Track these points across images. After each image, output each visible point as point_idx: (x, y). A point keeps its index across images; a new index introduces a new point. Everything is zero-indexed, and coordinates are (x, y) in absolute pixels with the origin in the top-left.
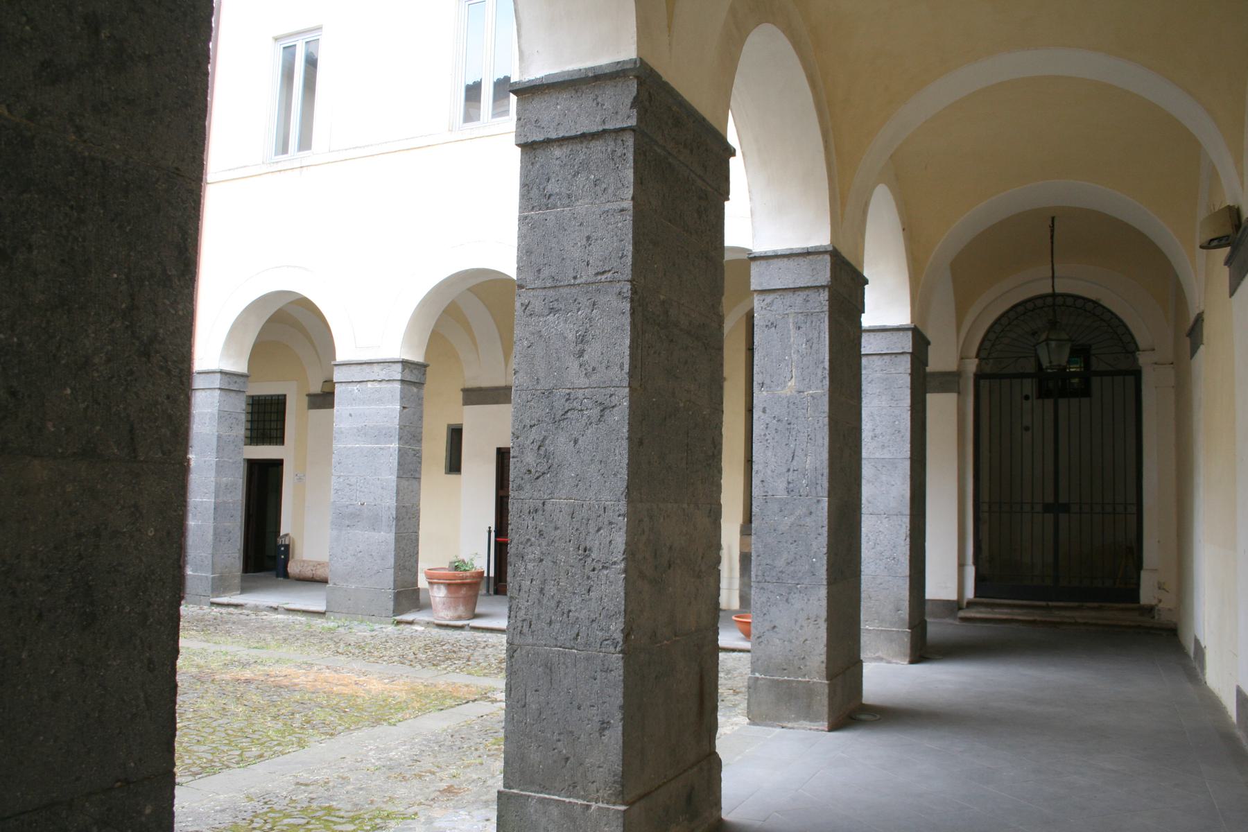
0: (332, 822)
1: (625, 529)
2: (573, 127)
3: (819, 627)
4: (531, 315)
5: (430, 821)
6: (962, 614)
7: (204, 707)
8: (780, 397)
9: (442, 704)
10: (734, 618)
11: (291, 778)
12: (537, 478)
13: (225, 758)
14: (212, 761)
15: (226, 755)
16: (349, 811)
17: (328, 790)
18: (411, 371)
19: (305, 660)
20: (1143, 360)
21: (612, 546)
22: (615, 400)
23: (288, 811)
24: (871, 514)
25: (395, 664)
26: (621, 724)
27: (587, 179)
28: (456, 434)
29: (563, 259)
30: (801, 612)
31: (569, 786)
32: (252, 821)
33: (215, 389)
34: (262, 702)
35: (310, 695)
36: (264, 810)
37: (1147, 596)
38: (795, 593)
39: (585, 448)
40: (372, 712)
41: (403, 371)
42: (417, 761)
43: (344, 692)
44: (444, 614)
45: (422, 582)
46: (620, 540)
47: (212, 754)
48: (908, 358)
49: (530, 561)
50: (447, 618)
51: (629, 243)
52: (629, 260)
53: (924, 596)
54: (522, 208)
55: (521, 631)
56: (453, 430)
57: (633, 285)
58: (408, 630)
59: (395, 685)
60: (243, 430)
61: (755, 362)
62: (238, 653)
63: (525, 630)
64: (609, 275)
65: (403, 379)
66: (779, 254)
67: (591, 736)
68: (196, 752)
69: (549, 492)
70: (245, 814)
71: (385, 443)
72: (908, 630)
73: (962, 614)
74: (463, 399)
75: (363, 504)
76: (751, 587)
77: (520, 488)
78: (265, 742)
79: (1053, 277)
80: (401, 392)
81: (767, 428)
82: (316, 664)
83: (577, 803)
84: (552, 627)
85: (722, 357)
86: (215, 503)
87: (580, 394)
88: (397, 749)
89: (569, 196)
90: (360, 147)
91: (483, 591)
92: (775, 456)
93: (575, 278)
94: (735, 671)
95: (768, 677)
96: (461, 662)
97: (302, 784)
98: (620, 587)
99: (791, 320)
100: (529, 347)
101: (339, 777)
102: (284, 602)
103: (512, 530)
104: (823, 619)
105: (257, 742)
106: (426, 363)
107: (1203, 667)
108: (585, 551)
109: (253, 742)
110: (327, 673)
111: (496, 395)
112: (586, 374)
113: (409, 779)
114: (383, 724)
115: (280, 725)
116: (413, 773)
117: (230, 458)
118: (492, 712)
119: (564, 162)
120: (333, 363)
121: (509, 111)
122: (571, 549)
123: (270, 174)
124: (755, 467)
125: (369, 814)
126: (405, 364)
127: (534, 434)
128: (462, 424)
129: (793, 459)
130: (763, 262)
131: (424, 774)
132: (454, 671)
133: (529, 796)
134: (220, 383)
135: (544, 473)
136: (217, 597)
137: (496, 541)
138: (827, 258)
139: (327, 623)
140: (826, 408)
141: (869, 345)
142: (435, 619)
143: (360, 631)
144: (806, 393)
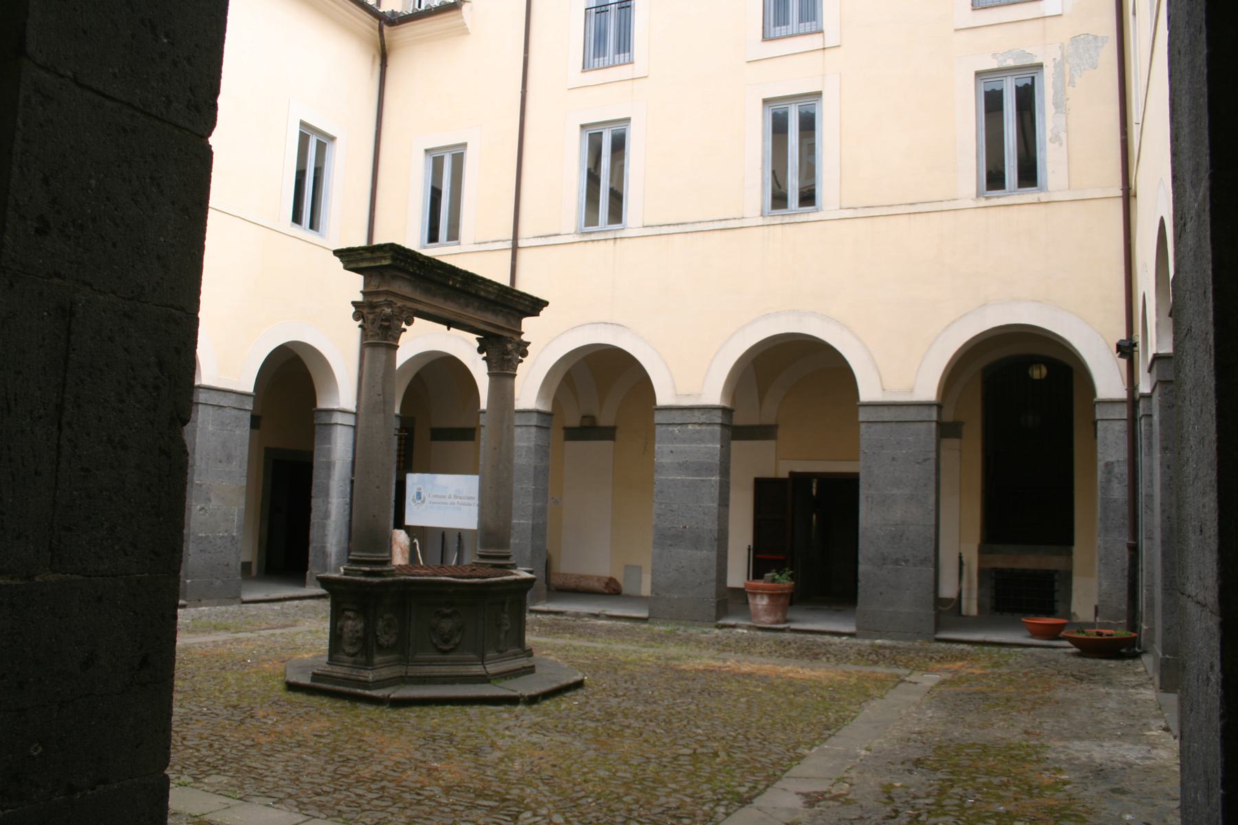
33: (531, 426)
44: (766, 620)
65: (1163, 379)
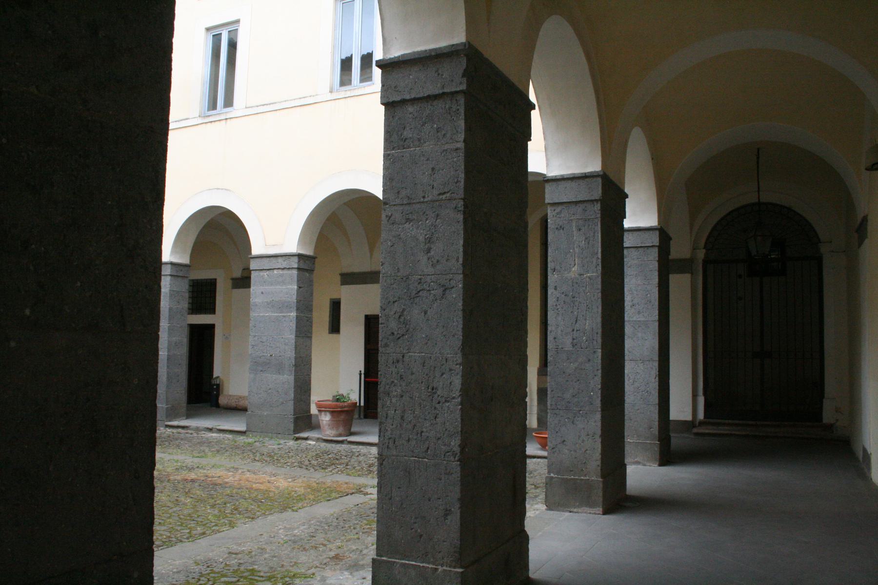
0: (255, 580)
1: (461, 373)
2: (421, 91)
3: (596, 441)
4: (393, 223)
5: (324, 579)
6: (695, 430)
7: (163, 499)
8: (567, 278)
9: (330, 496)
10: (534, 434)
11: (225, 549)
12: (399, 338)
13: (179, 535)
14: (169, 537)
15: (179, 533)
16: (266, 573)
17: (251, 557)
18: (305, 261)
19: (232, 465)
20: (824, 249)
21: (452, 386)
22: (453, 283)
23: (224, 572)
24: (631, 360)
25: (296, 468)
26: (459, 511)
27: (432, 127)
28: (336, 306)
29: (416, 184)
30: (583, 430)
31: (423, 555)
32: (199, 580)
33: (167, 275)
34: (203, 495)
35: (237, 490)
36: (207, 572)
37: (828, 417)
38: (578, 417)
39: (432, 317)
40: (280, 502)
41: (299, 262)
42: (313, 536)
43: (260, 488)
44: (329, 433)
45: (314, 410)
46: (457, 382)
47: (170, 532)
48: (656, 250)
49: (394, 397)
50: (331, 435)
51: (462, 173)
52: (462, 184)
53: (669, 418)
54: (386, 148)
55: (388, 446)
56: (334, 302)
57: (464, 202)
58: (304, 444)
59: (295, 483)
60: (187, 304)
61: (549, 254)
62: (186, 460)
63: (391, 445)
64: (448, 195)
66: (565, 177)
67: (438, 520)
68: (159, 531)
69: (407, 348)
70: (194, 574)
71: (287, 312)
72: (657, 442)
73: (695, 430)
74: (341, 281)
75: (271, 356)
76: (547, 413)
77: (386, 345)
78: (207, 523)
79: (759, 191)
80: (298, 276)
81: (557, 301)
82: (241, 469)
83: (428, 567)
84: (410, 443)
85: (527, 252)
86: (168, 355)
87: (428, 279)
88: (299, 528)
89: (419, 140)
90: (267, 105)
91: (356, 416)
92: (564, 320)
93: (424, 197)
94: (535, 472)
95: (559, 476)
96: (342, 466)
97: (233, 553)
98: (458, 415)
99: (574, 224)
100: (392, 246)
101: (259, 548)
102: (217, 424)
103: (381, 375)
104: (599, 435)
105: (201, 523)
106: (315, 256)
107: (869, 468)
108: (433, 389)
109: (198, 523)
110: (248, 475)
111: (368, 278)
112: (432, 265)
113: (308, 550)
114: (288, 511)
115: (216, 512)
116: (311, 545)
117: (178, 324)
118: (365, 501)
119: (415, 116)
120: (250, 256)
121: (372, 77)
122: (423, 388)
123: (209, 124)
124: (549, 328)
125: (281, 574)
126: (300, 256)
127: (396, 308)
128: (340, 299)
129: (576, 323)
130: (554, 184)
131: (318, 546)
132: (337, 473)
133: (394, 562)
134: (171, 272)
135: (403, 335)
136: (170, 421)
137: (365, 381)
138: (600, 180)
139: (247, 439)
140: (600, 287)
141: (629, 241)
142: (323, 436)
143: (271, 445)
144: (585, 276)
